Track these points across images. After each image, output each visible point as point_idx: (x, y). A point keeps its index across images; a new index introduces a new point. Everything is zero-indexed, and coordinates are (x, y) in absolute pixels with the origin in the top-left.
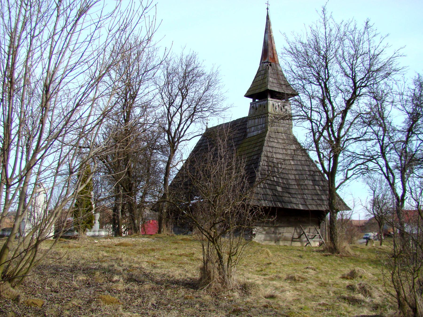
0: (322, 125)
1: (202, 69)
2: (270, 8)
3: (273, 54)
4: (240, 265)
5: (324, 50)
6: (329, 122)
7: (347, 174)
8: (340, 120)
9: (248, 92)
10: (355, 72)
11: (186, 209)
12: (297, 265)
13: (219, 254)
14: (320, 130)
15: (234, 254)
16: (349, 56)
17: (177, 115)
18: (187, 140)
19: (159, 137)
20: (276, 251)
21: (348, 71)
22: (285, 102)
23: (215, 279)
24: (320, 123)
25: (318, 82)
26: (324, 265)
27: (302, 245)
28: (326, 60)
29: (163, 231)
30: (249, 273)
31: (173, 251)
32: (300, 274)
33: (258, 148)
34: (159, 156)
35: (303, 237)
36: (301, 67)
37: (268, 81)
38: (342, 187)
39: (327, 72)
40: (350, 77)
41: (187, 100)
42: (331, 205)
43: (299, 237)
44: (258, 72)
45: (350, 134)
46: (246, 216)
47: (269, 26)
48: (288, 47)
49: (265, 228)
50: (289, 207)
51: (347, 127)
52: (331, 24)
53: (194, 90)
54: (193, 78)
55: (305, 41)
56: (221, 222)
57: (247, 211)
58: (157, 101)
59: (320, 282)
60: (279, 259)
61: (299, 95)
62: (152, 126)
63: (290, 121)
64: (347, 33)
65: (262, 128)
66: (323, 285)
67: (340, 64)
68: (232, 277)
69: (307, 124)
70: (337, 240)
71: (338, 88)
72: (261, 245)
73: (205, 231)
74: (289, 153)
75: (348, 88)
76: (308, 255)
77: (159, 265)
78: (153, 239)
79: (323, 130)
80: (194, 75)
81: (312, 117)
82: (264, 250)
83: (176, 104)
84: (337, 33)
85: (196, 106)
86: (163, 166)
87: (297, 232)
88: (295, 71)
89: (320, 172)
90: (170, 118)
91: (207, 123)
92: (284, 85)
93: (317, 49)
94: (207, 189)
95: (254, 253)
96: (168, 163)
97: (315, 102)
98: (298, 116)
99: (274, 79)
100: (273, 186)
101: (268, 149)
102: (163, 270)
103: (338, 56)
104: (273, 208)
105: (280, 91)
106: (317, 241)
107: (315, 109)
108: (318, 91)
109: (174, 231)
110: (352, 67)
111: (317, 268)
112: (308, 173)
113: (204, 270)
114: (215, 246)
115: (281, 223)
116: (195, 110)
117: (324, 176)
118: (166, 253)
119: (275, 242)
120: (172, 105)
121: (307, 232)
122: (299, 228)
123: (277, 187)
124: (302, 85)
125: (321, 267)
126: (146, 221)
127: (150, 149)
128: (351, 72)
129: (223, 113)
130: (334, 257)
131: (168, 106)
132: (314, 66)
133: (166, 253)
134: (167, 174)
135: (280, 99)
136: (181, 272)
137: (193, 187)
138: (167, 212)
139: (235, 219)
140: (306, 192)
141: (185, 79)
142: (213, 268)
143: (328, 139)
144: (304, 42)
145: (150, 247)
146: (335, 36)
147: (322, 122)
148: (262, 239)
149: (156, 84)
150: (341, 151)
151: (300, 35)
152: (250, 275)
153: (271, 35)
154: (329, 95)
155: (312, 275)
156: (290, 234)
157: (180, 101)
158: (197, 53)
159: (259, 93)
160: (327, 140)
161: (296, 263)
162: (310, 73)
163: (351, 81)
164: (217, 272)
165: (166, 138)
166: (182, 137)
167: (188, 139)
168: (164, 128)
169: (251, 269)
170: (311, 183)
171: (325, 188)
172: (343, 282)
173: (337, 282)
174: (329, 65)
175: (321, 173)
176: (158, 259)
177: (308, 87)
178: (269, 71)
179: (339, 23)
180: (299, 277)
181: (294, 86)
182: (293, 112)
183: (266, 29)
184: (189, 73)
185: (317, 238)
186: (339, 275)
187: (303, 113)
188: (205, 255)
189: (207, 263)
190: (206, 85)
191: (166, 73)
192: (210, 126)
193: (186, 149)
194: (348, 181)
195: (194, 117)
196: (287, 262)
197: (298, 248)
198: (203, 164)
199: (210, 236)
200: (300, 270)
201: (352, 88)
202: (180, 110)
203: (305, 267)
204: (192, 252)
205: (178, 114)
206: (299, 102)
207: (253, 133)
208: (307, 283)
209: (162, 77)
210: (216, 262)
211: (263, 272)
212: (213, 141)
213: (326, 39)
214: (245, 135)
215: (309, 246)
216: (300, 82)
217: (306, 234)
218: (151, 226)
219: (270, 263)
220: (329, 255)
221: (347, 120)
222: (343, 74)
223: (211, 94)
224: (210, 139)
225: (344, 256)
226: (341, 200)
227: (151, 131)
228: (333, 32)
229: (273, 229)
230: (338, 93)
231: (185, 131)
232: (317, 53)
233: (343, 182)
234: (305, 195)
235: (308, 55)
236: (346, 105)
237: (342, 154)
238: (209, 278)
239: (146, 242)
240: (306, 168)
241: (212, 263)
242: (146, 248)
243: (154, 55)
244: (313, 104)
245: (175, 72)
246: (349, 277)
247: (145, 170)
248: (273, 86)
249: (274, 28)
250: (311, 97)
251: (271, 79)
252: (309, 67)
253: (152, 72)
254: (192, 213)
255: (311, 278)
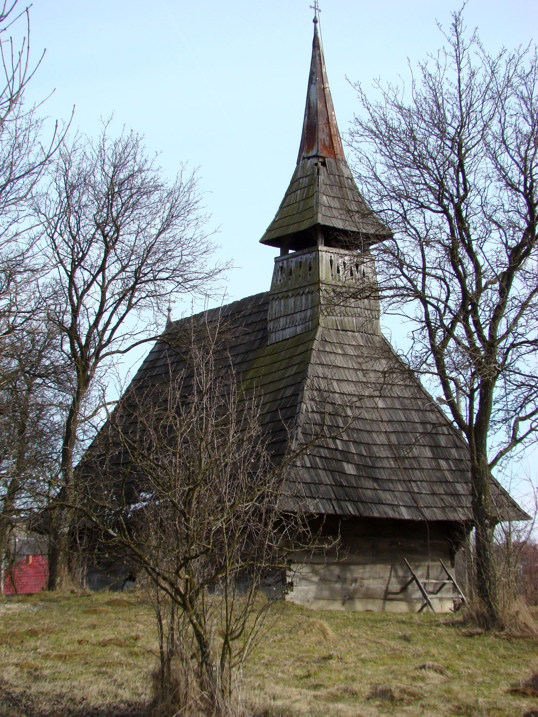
0: (450, 311)
1: (153, 176)
2: (321, 18)
3: (331, 136)
4: (255, 664)
5: (456, 124)
6: (469, 304)
7: (515, 429)
8: (496, 298)
9: (269, 230)
10: (531, 177)
11: (117, 525)
12: (396, 661)
13: (199, 636)
14: (447, 322)
15: (237, 633)
16: (517, 138)
17: (92, 289)
18: (118, 352)
19: (49, 345)
20: (345, 626)
21: (516, 175)
22: (358, 256)
23: (191, 702)
24: (446, 306)
25: (440, 204)
26: (464, 660)
27: (412, 610)
28: (460, 150)
29: (60, 584)
30: (277, 683)
31: (85, 633)
32: (405, 683)
33: (295, 368)
34: (49, 394)
35: (413, 587)
36: (397, 168)
37: (317, 203)
38: (505, 462)
39: (461, 180)
40: (519, 191)
41: (119, 251)
42: (478, 507)
43: (404, 589)
44: (292, 183)
45: (520, 330)
46: (265, 537)
47: (318, 67)
48: (365, 117)
49: (318, 567)
50: (376, 515)
51: (512, 315)
52: (474, 59)
53: (134, 227)
54: (131, 197)
55: (408, 103)
56: (202, 553)
57: (266, 525)
58: (40, 256)
59: (456, 703)
60: (353, 644)
61: (396, 236)
62: (29, 318)
63: (372, 302)
64: (515, 81)
65: (304, 321)
66: (463, 710)
67: (495, 158)
68: (234, 694)
69: (414, 307)
70: (495, 594)
71: (490, 218)
72: (307, 610)
73: (165, 579)
74: (373, 380)
75: (515, 217)
76: (425, 635)
77: (46, 672)
78: (35, 605)
79: (453, 324)
80: (134, 191)
81: (427, 292)
82: (313, 624)
83: (89, 262)
84: (488, 79)
85: (140, 268)
86: (59, 418)
87: (397, 577)
88: (382, 179)
89: (449, 424)
90: (75, 298)
91: (169, 310)
92: (357, 212)
93: (439, 124)
94: (167, 474)
95: (290, 632)
96: (73, 412)
97: (434, 254)
98: (391, 288)
99: (333, 197)
100: (333, 462)
101: (320, 370)
102: (59, 683)
103: (490, 138)
104: (333, 518)
105: (348, 228)
106: (448, 599)
107: (433, 272)
108: (439, 227)
109: (89, 582)
110: (525, 166)
111: (448, 668)
112: (420, 428)
113: (163, 680)
114: (190, 617)
115: (352, 552)
116: (137, 279)
117: (459, 437)
118: (66, 638)
119: (344, 603)
120: (79, 264)
121: (422, 576)
122: (402, 565)
123: (345, 464)
124: (401, 212)
125: (459, 664)
126: (18, 559)
127: (25, 377)
128: (522, 178)
129: (208, 285)
130: (490, 639)
131: (69, 268)
132: (429, 164)
133: (66, 639)
134: (69, 437)
135: (347, 248)
136: (105, 687)
137: (134, 468)
138: (71, 533)
139: (237, 546)
140: (418, 474)
141: (112, 202)
142: (186, 673)
143: (466, 343)
144: (406, 106)
145: (27, 627)
146: (484, 89)
147: (451, 303)
148: (311, 595)
149: (38, 210)
150: (499, 372)
151: (394, 87)
152: (278, 689)
153: (324, 89)
154: (469, 236)
155: (436, 686)
156: (381, 581)
157: (99, 256)
158: (140, 135)
159: (296, 234)
160: (465, 347)
161: (395, 656)
162: (420, 182)
163: (522, 200)
164: (195, 684)
165: (67, 347)
166: (106, 345)
167: (122, 349)
168: (61, 324)
169: (283, 672)
170: (428, 453)
171: (462, 466)
172: (513, 703)
173: (499, 705)
174: (467, 161)
175: (453, 429)
176: (46, 657)
177: (416, 218)
178: (321, 178)
179: (494, 57)
180: (403, 691)
181: (382, 215)
182: (379, 278)
183: (312, 73)
184: (121, 184)
185: (448, 591)
186: (505, 686)
187: (405, 280)
188: (164, 639)
189: (169, 660)
190: (165, 215)
191: (62, 185)
192: (176, 317)
193: (116, 375)
194: (519, 446)
195: (136, 294)
196: (371, 652)
197: (399, 617)
198: (155, 411)
199: (177, 591)
200: (405, 674)
201: (525, 218)
202: (100, 278)
203: (417, 666)
204: (134, 634)
205: (95, 289)
206: (393, 254)
207: (282, 332)
208: (423, 706)
209: (54, 196)
210: (192, 657)
211: (313, 681)
212: (186, 353)
213: (460, 96)
214: (264, 338)
215: (428, 612)
216: (396, 206)
217: (421, 581)
218: (31, 571)
219: (330, 657)
220: (479, 634)
221: (514, 298)
222: (502, 184)
223: (177, 237)
224: (177, 350)
225: (515, 637)
226: (504, 493)
227: (27, 332)
228: (479, 79)
229: (336, 570)
230: (491, 232)
231: (114, 330)
232: (437, 131)
233: (506, 450)
234: (413, 484)
235: (414, 139)
236: (510, 261)
237: (503, 380)
238: (176, 700)
239: (14, 614)
240: (415, 417)
241: (182, 660)
242: (14, 629)
243: (31, 140)
244: (427, 259)
245: (85, 181)
246: (529, 691)
247: (15, 428)
248: (330, 214)
249: (331, 70)
250: (423, 242)
251: (324, 197)
252: (418, 168)
253: (27, 180)
254: (129, 533)
255: (431, 692)
